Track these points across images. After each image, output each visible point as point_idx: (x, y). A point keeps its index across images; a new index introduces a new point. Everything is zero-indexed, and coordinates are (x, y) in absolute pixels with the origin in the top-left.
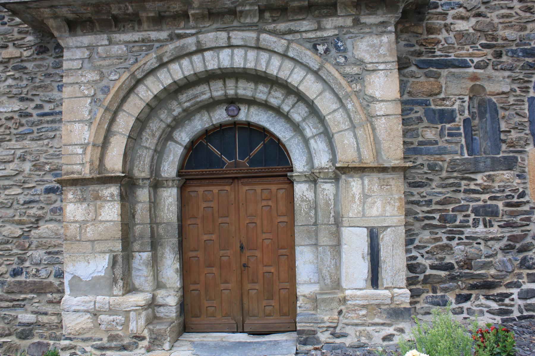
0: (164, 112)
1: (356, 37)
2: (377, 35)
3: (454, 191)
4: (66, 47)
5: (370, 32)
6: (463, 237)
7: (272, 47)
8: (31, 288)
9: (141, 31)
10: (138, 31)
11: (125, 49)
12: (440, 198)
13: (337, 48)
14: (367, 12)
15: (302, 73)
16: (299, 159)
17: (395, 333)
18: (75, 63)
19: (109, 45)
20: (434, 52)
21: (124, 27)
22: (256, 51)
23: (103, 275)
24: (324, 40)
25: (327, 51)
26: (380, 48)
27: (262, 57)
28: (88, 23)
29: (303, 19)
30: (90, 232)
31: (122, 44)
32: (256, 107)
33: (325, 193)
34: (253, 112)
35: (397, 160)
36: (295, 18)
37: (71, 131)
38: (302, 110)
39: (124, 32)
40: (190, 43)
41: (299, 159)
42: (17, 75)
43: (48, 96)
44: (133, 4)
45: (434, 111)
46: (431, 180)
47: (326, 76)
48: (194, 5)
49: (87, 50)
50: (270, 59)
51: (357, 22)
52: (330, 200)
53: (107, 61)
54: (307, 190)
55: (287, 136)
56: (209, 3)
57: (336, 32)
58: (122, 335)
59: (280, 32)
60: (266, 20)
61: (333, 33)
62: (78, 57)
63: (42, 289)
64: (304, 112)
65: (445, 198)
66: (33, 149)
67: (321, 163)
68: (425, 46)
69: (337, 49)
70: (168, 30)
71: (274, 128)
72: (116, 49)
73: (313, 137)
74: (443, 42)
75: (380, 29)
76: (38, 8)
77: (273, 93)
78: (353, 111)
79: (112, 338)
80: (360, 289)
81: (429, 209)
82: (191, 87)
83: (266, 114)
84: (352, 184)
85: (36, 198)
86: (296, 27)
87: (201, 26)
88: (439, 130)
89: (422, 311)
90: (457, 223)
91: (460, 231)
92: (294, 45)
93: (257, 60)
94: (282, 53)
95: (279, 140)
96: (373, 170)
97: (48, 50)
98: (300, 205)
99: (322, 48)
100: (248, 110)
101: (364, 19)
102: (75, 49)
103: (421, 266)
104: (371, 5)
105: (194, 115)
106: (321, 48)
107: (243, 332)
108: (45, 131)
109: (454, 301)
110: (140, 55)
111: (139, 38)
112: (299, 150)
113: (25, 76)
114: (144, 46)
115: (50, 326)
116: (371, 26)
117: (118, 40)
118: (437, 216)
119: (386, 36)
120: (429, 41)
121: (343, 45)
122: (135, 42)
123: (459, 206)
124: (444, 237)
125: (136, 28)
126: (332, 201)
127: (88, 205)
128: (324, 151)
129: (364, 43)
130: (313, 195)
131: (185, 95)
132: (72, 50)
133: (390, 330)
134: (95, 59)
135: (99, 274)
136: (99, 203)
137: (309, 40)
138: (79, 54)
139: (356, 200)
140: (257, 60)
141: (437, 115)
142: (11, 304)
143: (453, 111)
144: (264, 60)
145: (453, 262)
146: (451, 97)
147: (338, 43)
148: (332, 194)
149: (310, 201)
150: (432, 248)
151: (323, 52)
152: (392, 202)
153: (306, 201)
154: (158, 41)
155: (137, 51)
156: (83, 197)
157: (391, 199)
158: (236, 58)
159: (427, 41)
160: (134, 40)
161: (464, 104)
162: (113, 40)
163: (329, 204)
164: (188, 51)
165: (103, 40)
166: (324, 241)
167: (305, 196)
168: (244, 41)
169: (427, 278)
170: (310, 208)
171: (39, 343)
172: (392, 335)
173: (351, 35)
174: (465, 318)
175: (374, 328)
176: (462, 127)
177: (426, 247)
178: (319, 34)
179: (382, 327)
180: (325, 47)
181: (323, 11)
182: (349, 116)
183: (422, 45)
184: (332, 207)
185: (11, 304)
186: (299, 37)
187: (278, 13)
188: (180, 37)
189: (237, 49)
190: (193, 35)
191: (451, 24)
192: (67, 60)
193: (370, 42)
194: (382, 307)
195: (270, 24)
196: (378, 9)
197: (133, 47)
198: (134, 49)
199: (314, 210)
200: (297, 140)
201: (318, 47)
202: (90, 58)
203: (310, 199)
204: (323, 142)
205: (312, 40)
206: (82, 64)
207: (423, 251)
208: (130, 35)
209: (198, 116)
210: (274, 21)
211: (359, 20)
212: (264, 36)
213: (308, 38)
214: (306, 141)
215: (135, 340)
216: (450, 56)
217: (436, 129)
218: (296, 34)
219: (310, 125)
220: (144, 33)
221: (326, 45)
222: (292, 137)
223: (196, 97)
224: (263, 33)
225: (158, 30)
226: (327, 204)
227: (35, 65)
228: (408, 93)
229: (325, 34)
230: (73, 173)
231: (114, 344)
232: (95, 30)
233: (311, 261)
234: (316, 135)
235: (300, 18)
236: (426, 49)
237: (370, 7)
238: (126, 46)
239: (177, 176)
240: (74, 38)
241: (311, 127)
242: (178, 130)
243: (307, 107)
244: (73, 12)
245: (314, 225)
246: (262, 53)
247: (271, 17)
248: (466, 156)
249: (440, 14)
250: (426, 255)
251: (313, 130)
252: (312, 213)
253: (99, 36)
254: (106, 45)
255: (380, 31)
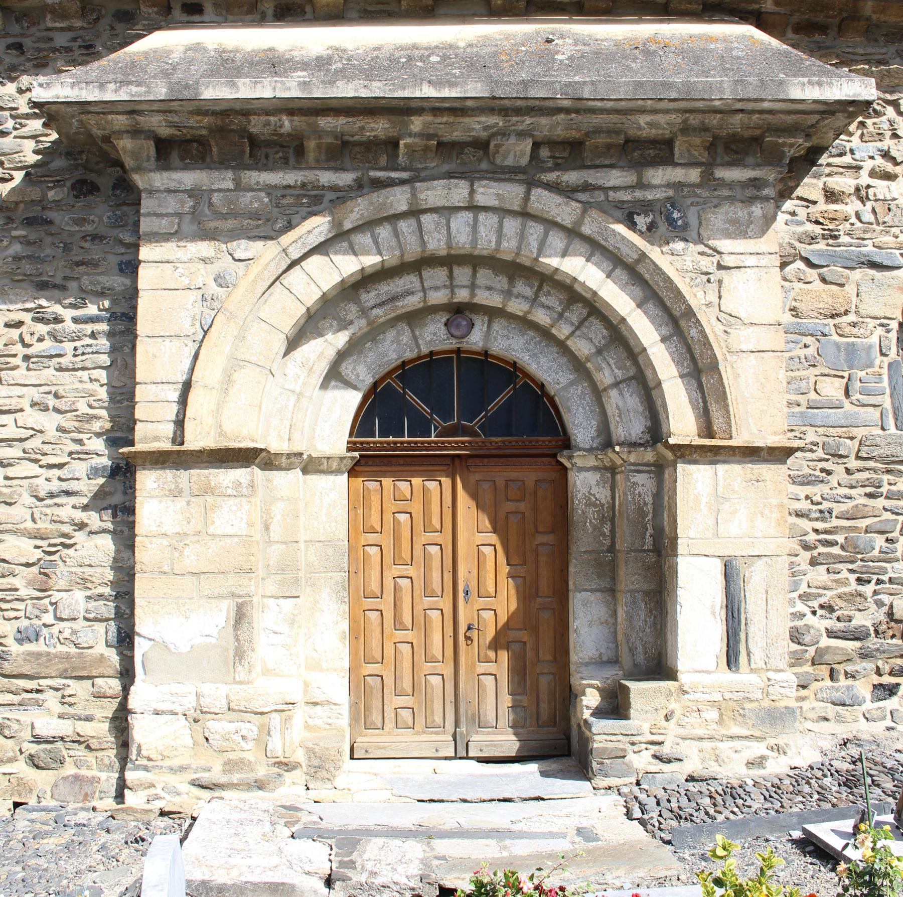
0: (331, 325)
1: (705, 203)
2: (743, 202)
3: (866, 495)
4: (145, 190)
5: (730, 196)
6: (885, 578)
7: (552, 213)
8: (60, 666)
9: (301, 169)
10: (295, 168)
11: (266, 200)
12: (848, 506)
13: (671, 222)
14: (727, 158)
15: (605, 264)
16: (585, 424)
17: (769, 753)
18: (164, 222)
19: (235, 190)
20: (836, 237)
21: (267, 157)
22: (519, 220)
23: (214, 641)
24: (646, 207)
25: (651, 227)
26: (748, 227)
27: (531, 231)
28: (195, 145)
29: (612, 166)
30: (191, 559)
31: (260, 190)
32: (503, 321)
33: (637, 492)
34: (497, 332)
35: (775, 433)
36: (597, 162)
37: (154, 356)
38: (596, 333)
39: (265, 168)
40: (399, 199)
41: (585, 424)
42: (32, 237)
43: (99, 283)
44: (295, 118)
45: (837, 345)
46: (829, 473)
47: (651, 275)
48: (412, 127)
49: (190, 197)
50: (546, 235)
51: (707, 178)
52: (646, 504)
53: (230, 222)
54: (598, 484)
55: (561, 380)
56: (442, 126)
57: (670, 193)
58: (252, 759)
59: (568, 186)
60: (544, 162)
61: (664, 195)
62: (170, 210)
63: (84, 668)
64: (600, 336)
65: (857, 506)
66: (67, 387)
67: (630, 434)
68: (822, 224)
69: (670, 224)
70: (355, 169)
71: (538, 363)
72: (249, 199)
73: (616, 384)
74: (853, 220)
75: (749, 192)
76: (104, 113)
77: (543, 299)
78: (699, 340)
79: (230, 766)
80: (708, 672)
81: (826, 525)
82: (385, 279)
83: (523, 335)
84: (695, 476)
85: (72, 486)
86: (597, 179)
87: (419, 166)
88: (846, 380)
89: (813, 715)
90: (876, 553)
91: (881, 568)
92: (594, 213)
93: (522, 236)
94: (569, 226)
95: (542, 386)
96: (734, 452)
97: (97, 189)
98: (583, 513)
99: (643, 221)
100: (489, 326)
101: (722, 173)
102: (165, 194)
103: (812, 631)
104: (734, 147)
105: (384, 333)
106: (642, 221)
107: (467, 758)
108: (93, 353)
109: (868, 696)
110: (297, 213)
111: (296, 181)
112: (584, 408)
113: (48, 240)
114: (305, 196)
115: (100, 743)
116: (731, 185)
117: (253, 181)
118: (840, 538)
119: (759, 206)
120: (831, 216)
121: (681, 218)
122: (289, 187)
123: (880, 521)
124: (852, 578)
125: (292, 160)
126: (649, 506)
127: (188, 503)
128: (637, 412)
129: (720, 217)
130: (609, 493)
131: (373, 294)
132: (157, 195)
133: (758, 749)
134: (206, 216)
135: (209, 640)
136: (210, 499)
137: (619, 205)
138: (172, 204)
139: (702, 507)
140: (522, 236)
141: (843, 353)
142: (16, 699)
143: (870, 347)
144: (535, 236)
145: (868, 624)
146: (866, 320)
147: (673, 213)
148: (650, 494)
149: (602, 505)
150: (832, 597)
151: (645, 227)
152: (767, 511)
153: (595, 506)
154: (333, 188)
155: (289, 206)
156: (177, 487)
157: (765, 506)
158: (482, 231)
159: (826, 215)
160: (285, 183)
161: (890, 335)
162: (244, 181)
163: (643, 512)
164: (391, 212)
165: (223, 179)
166: (633, 583)
167: (594, 495)
168: (499, 200)
169: (820, 652)
170: (603, 519)
171: (76, 777)
172: (763, 758)
173: (697, 199)
174: (888, 729)
175: (731, 744)
176: (885, 378)
177: (820, 596)
178: (639, 194)
179: (746, 743)
180: (649, 220)
181: (648, 152)
182: (689, 350)
183: (817, 222)
184: (650, 517)
185: (16, 699)
186: (603, 198)
187: (564, 150)
188: (379, 184)
189: (484, 214)
190: (402, 182)
191: (868, 187)
192: (149, 215)
193: (731, 214)
194: (747, 705)
195: (551, 170)
196: (747, 154)
197: (284, 196)
198: (284, 202)
199: (609, 523)
200: (580, 388)
201: (637, 219)
202: (194, 212)
203: (603, 501)
204: (634, 396)
205: (626, 206)
206: (179, 224)
207: (815, 604)
208: (280, 174)
209: (391, 335)
210: (557, 167)
211: (712, 174)
212: (538, 193)
213: (620, 202)
214: (598, 394)
215: (279, 770)
216: (866, 246)
217: (840, 379)
218: (596, 192)
219: (612, 362)
220: (306, 173)
221: (651, 216)
222: (572, 383)
223: (394, 298)
224: (538, 186)
225: (336, 169)
226: (641, 512)
227: (70, 218)
228: (791, 310)
229: (650, 195)
230: (156, 439)
231: (236, 778)
232: (208, 160)
233: (602, 620)
234: (621, 382)
235: (607, 162)
236: (824, 230)
237: (732, 150)
238: (268, 194)
239: (349, 450)
240: (165, 174)
241: (613, 366)
242: (351, 360)
243: (606, 329)
244: (172, 125)
245: (608, 551)
246: (531, 223)
247: (551, 157)
248: (892, 430)
249: (849, 167)
250: (820, 612)
251: (616, 371)
252: (606, 529)
253: (216, 174)
254: (228, 190)
255: (749, 195)
